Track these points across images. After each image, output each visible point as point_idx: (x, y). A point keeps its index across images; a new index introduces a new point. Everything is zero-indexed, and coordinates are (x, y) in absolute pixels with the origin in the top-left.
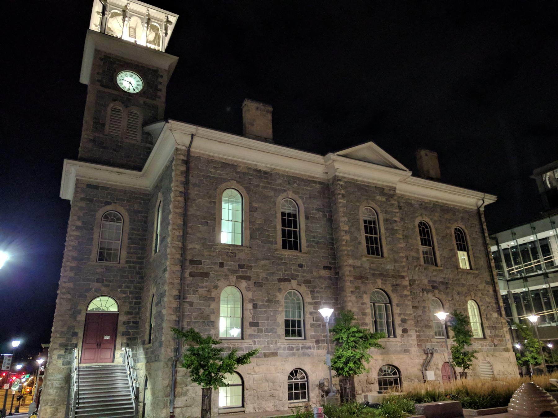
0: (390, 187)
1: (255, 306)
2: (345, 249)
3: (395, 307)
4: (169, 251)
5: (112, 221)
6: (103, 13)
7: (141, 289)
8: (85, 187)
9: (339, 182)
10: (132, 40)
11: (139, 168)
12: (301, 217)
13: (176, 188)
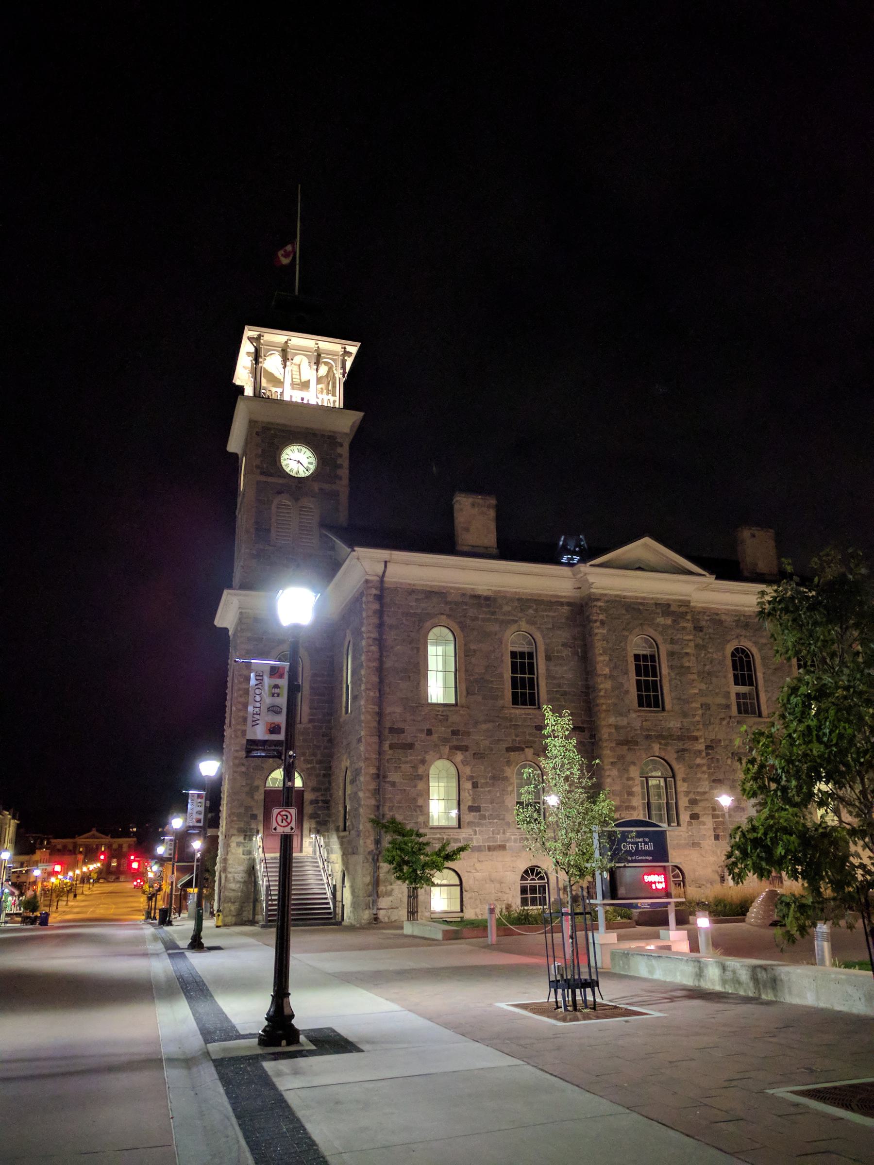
0: (680, 601)
1: (475, 785)
2: (604, 702)
3: (679, 783)
7: (331, 756)
9: (595, 603)
12: (539, 659)
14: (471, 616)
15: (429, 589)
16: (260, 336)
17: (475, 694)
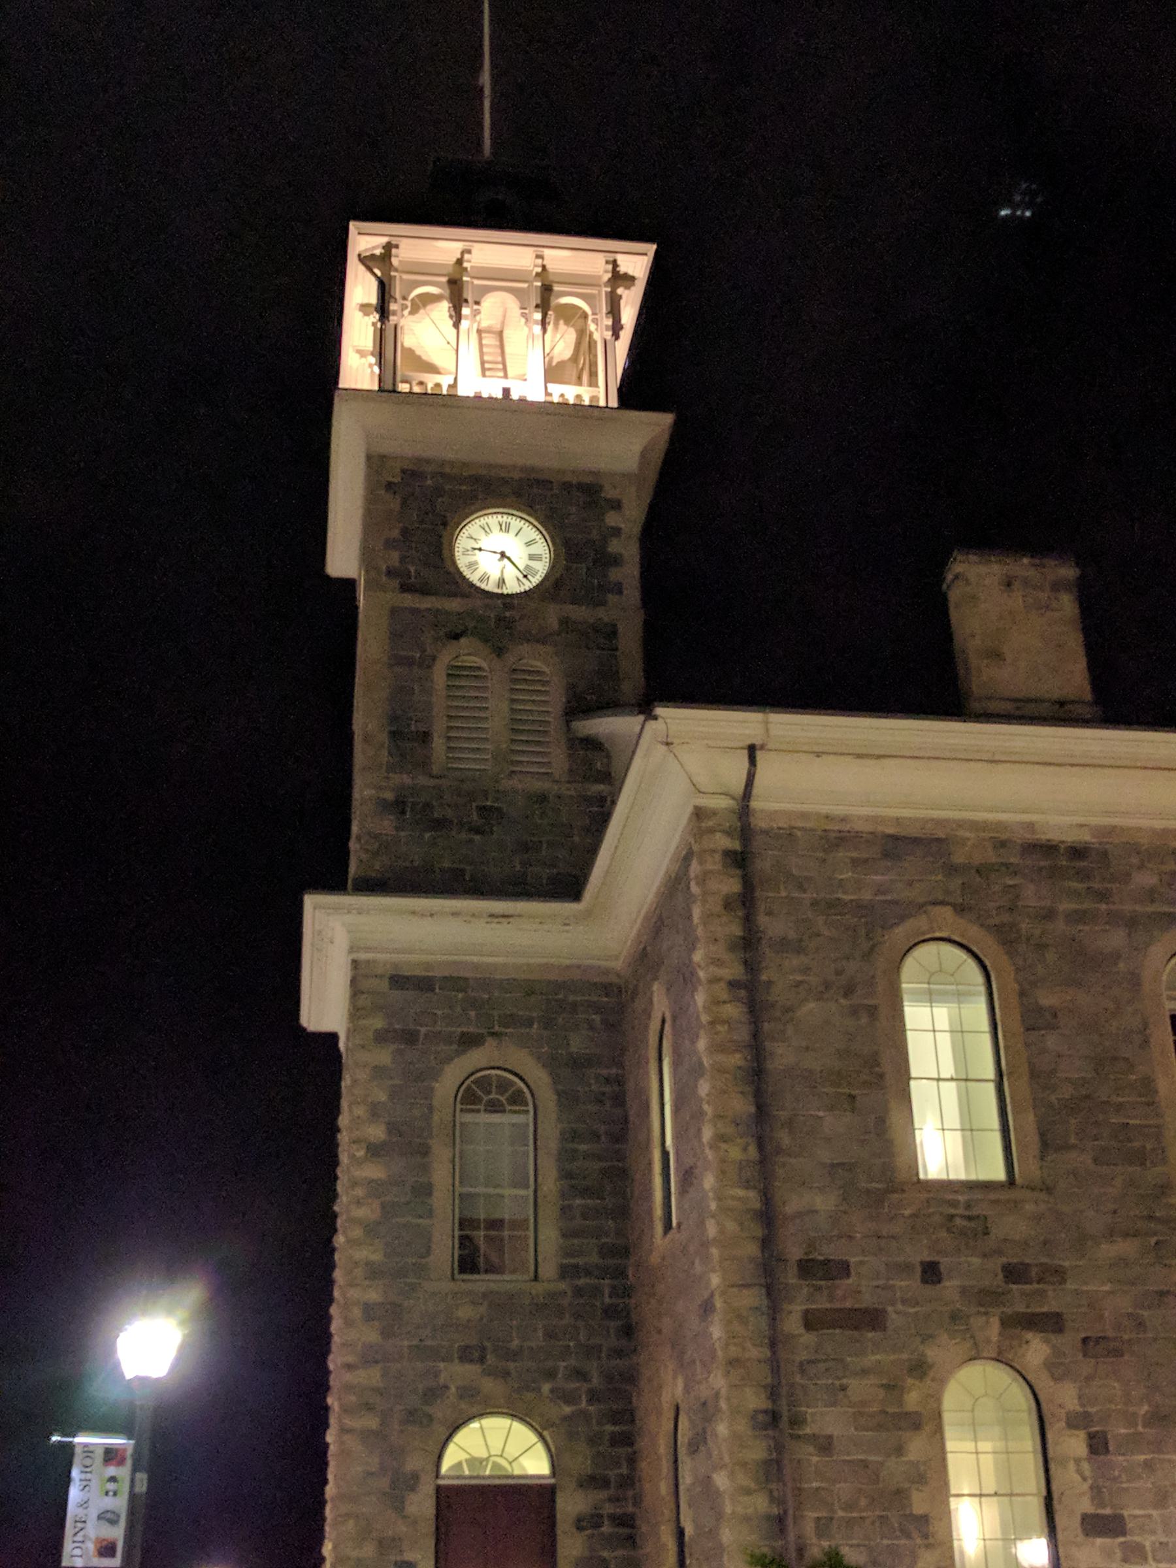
1: (1098, 1445)
4: (712, 1229)
5: (495, 1107)
6: (383, 309)
7: (631, 1377)
8: (384, 985)
10: (492, 388)
11: (569, 887)
13: (712, 968)
14: (1035, 908)
15: (891, 831)
16: (388, 247)
17: (1067, 1147)
